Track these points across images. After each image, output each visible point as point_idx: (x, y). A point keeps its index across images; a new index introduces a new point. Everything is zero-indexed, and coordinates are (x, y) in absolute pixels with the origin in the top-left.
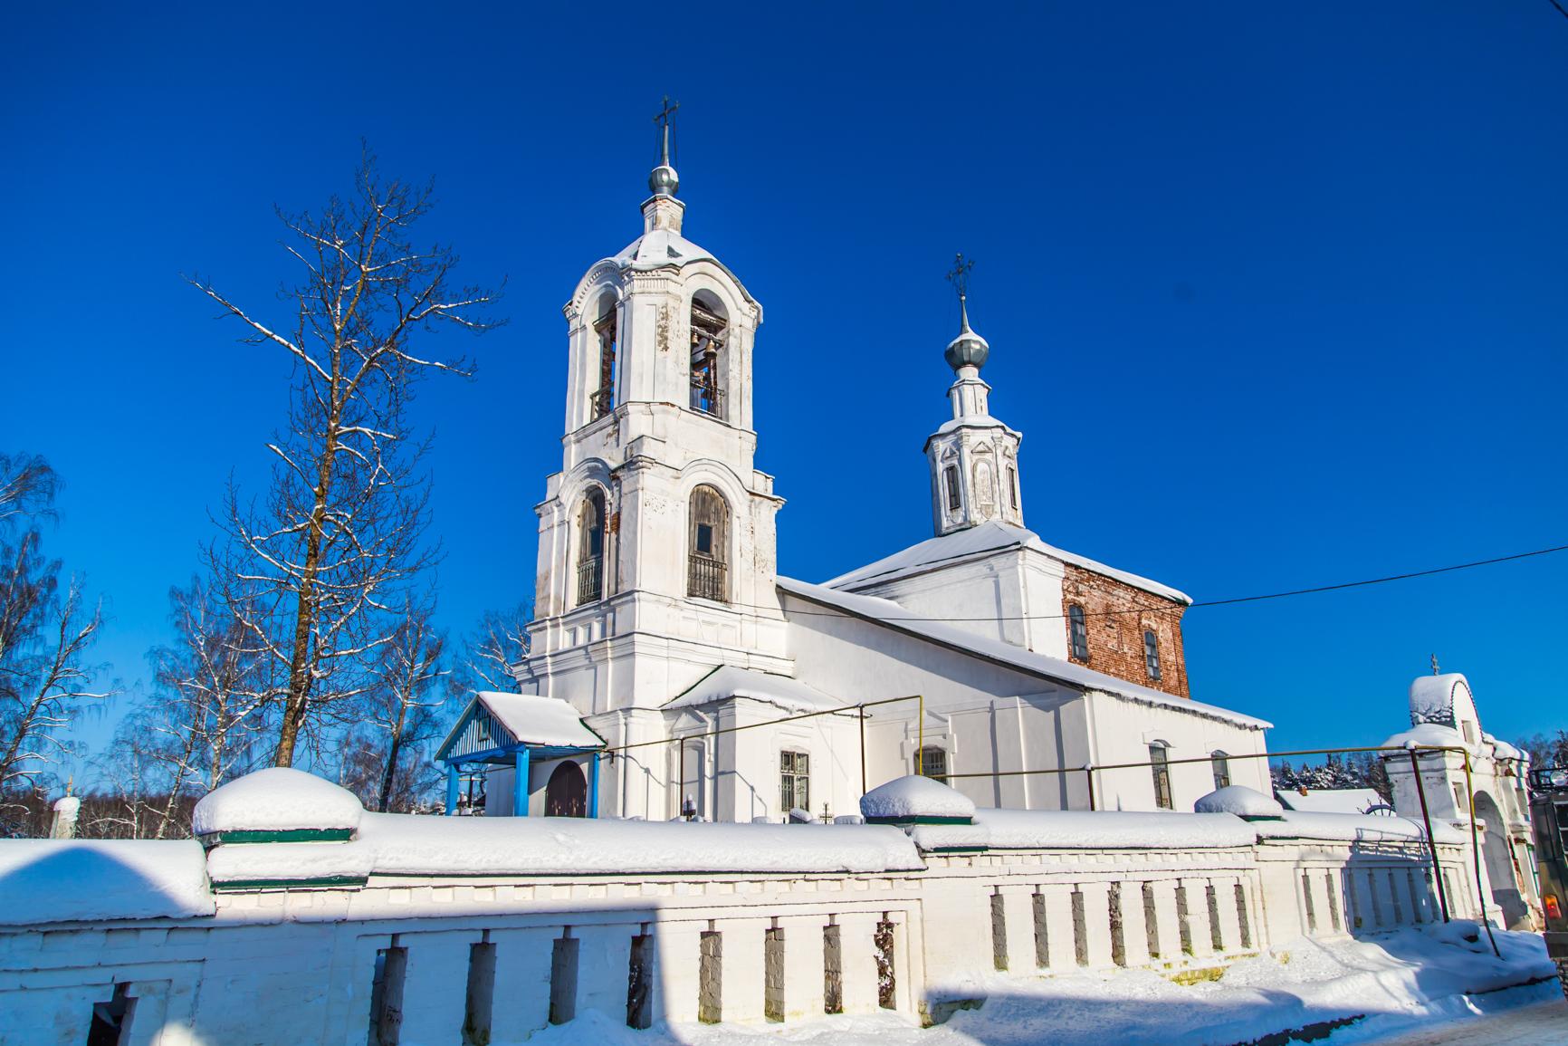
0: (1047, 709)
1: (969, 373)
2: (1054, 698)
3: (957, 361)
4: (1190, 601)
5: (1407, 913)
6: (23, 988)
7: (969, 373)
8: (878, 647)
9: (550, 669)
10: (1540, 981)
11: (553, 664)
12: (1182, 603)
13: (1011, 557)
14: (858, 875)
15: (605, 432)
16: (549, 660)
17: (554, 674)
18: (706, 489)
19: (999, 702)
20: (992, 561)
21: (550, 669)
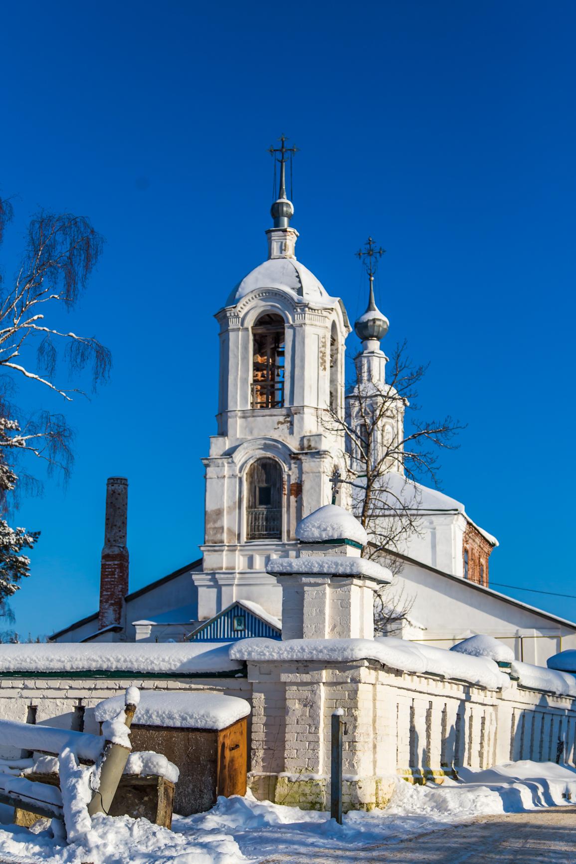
0: (551, 637)
1: (374, 345)
2: (559, 633)
3: (366, 333)
4: (498, 544)
5: (548, 718)
6: (71, 688)
7: (374, 345)
8: (435, 587)
9: (236, 582)
10: (445, 709)
11: (240, 579)
12: (492, 545)
13: (449, 518)
14: (542, 738)
15: (276, 419)
16: (237, 576)
17: (238, 585)
18: (265, 461)
19: (523, 632)
20: (433, 518)
21: (236, 582)
